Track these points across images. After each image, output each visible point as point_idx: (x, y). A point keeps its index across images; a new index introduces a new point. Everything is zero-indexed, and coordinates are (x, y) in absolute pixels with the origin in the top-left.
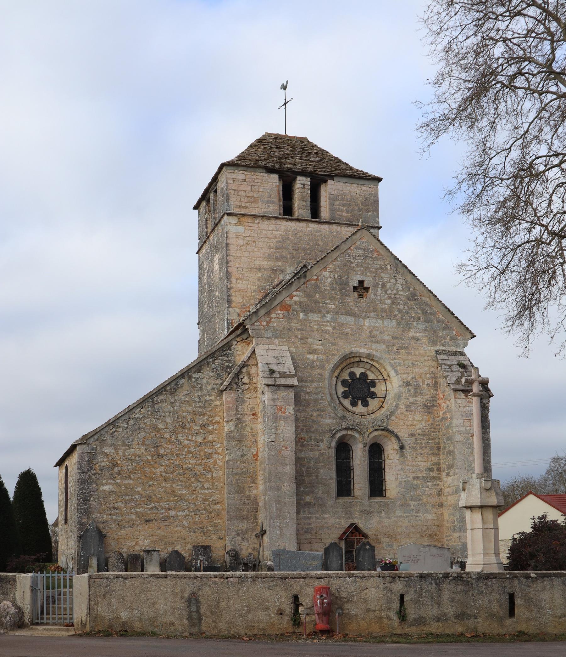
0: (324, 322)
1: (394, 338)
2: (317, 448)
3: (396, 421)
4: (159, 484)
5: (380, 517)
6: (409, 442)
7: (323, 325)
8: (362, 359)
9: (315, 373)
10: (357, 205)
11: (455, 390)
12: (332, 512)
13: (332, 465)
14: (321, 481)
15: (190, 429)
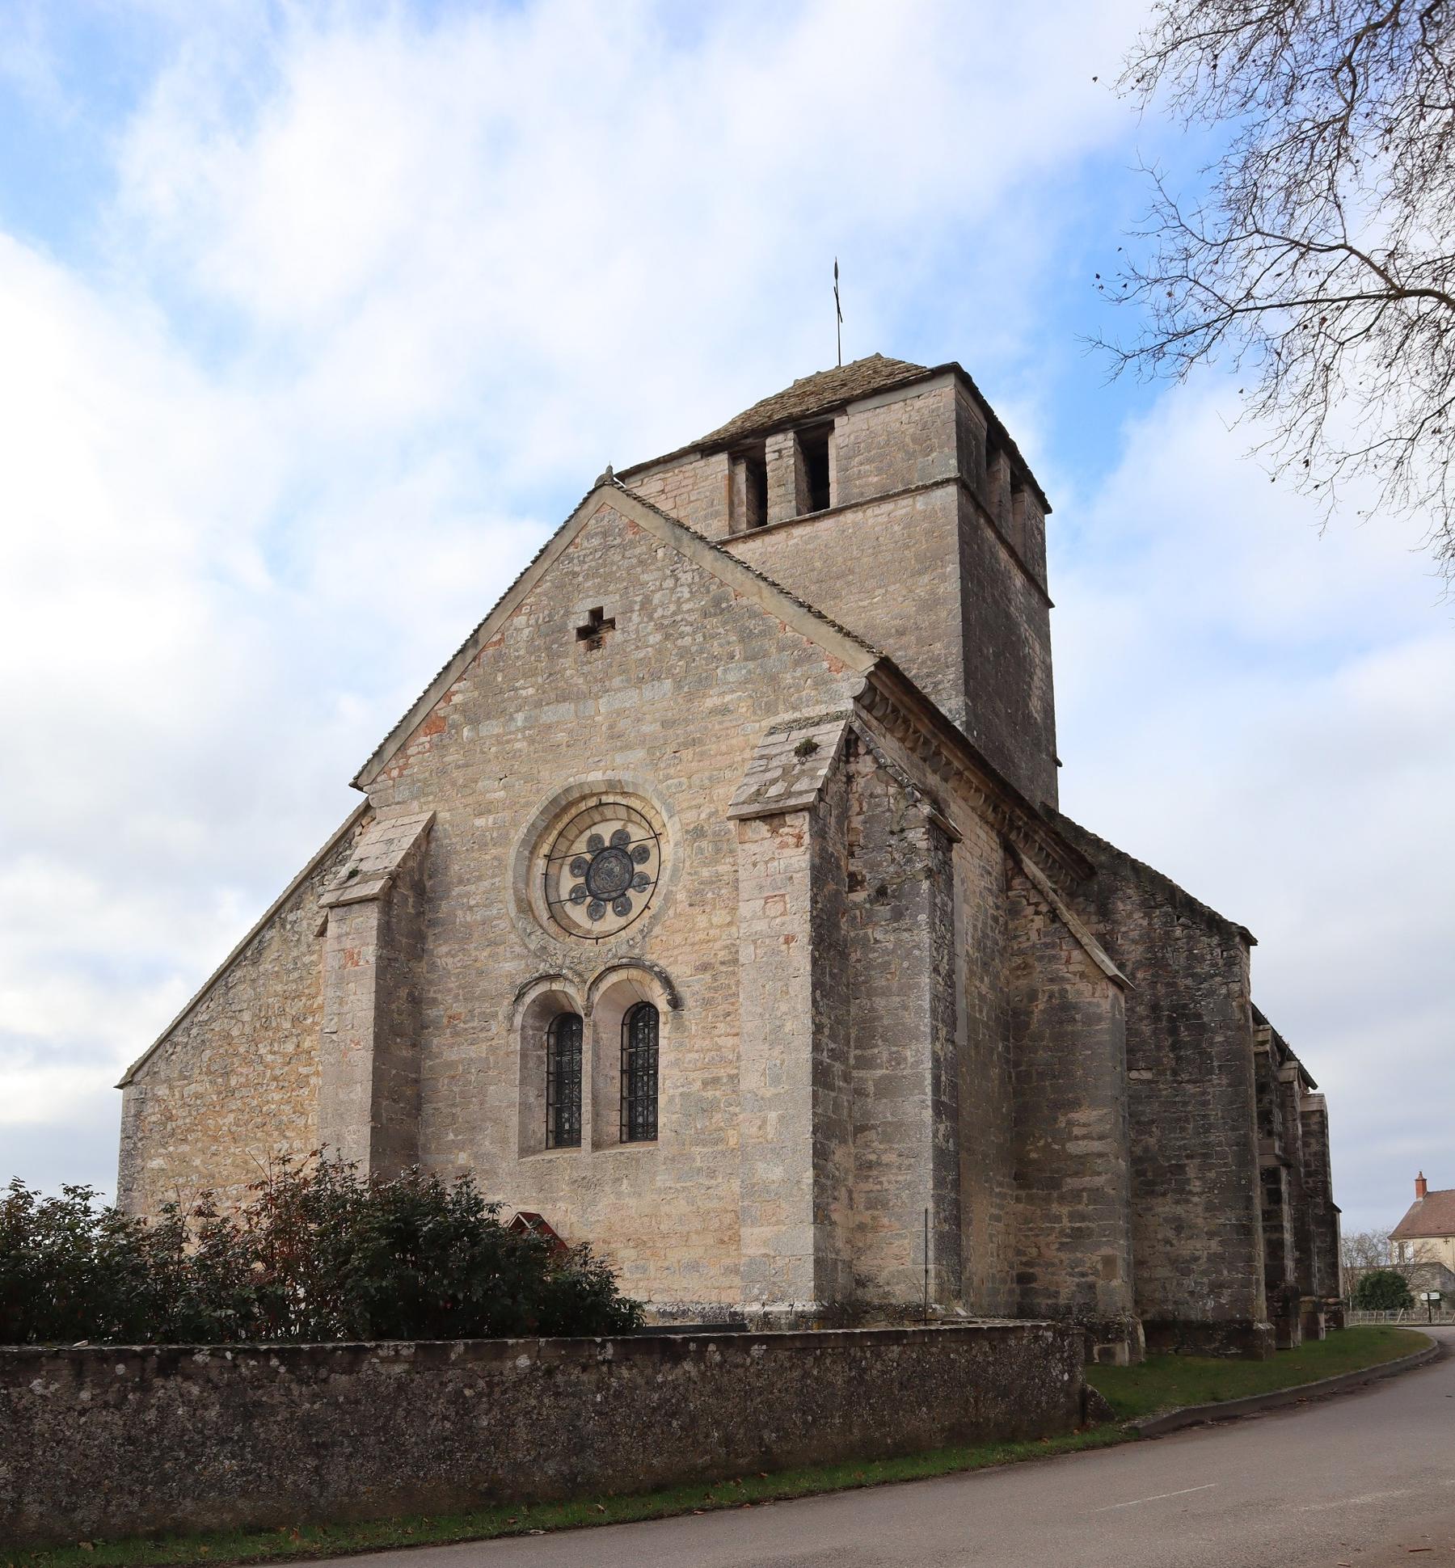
0: (510, 733)
1: (665, 724)
2: (482, 1035)
3: (664, 938)
4: (226, 1149)
5: (619, 1195)
7: (508, 742)
8: (605, 799)
9: (488, 857)
10: (902, 447)
11: (744, 819)
12: (509, 1188)
15: (278, 1029)
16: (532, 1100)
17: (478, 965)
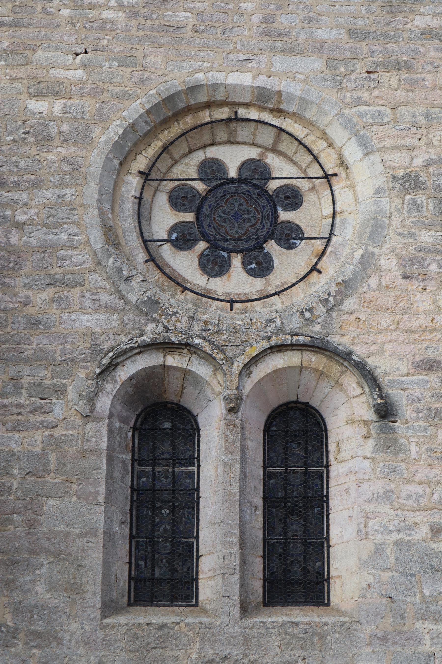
2: (35, 418)
3: (363, 317)
6: (417, 392)
8: (242, 112)
13: (96, 483)
14: (46, 544)
16: (116, 528)
17: (29, 310)
